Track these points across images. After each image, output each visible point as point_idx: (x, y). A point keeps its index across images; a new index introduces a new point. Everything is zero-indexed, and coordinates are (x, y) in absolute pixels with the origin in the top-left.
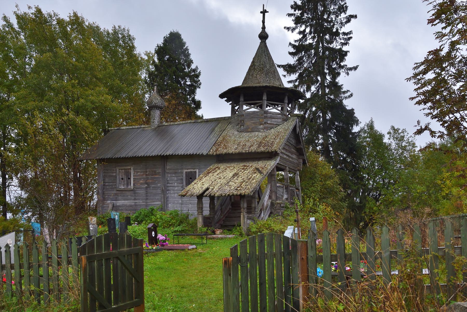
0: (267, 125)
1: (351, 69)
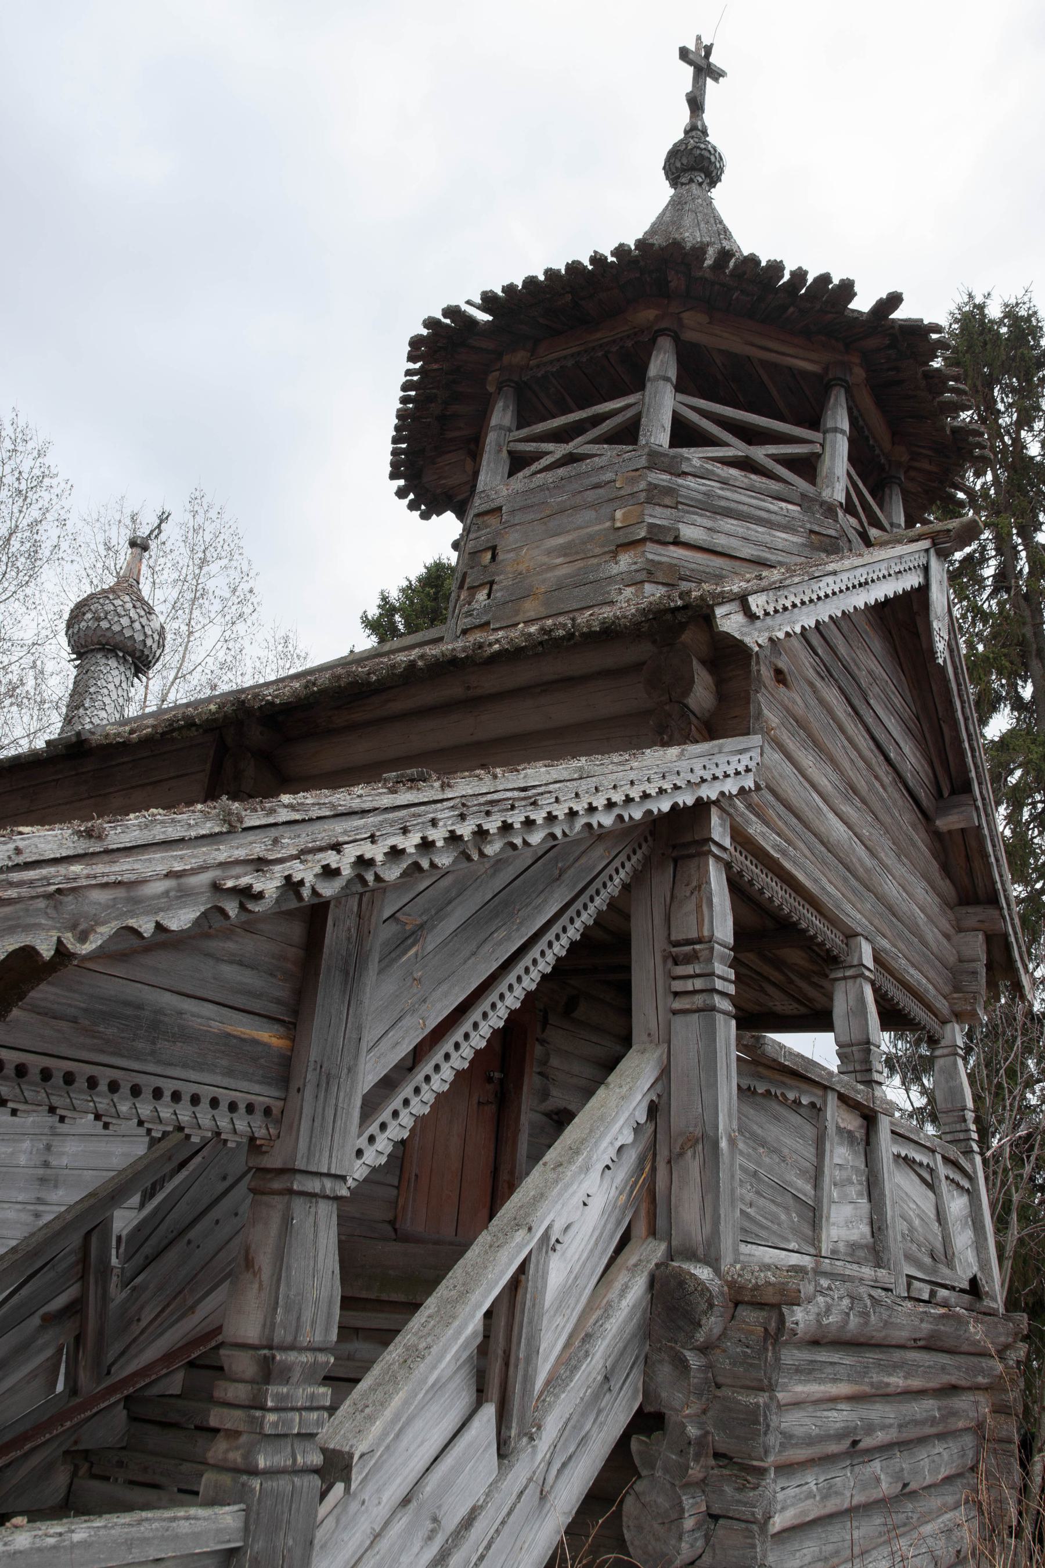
0: (677, 553)
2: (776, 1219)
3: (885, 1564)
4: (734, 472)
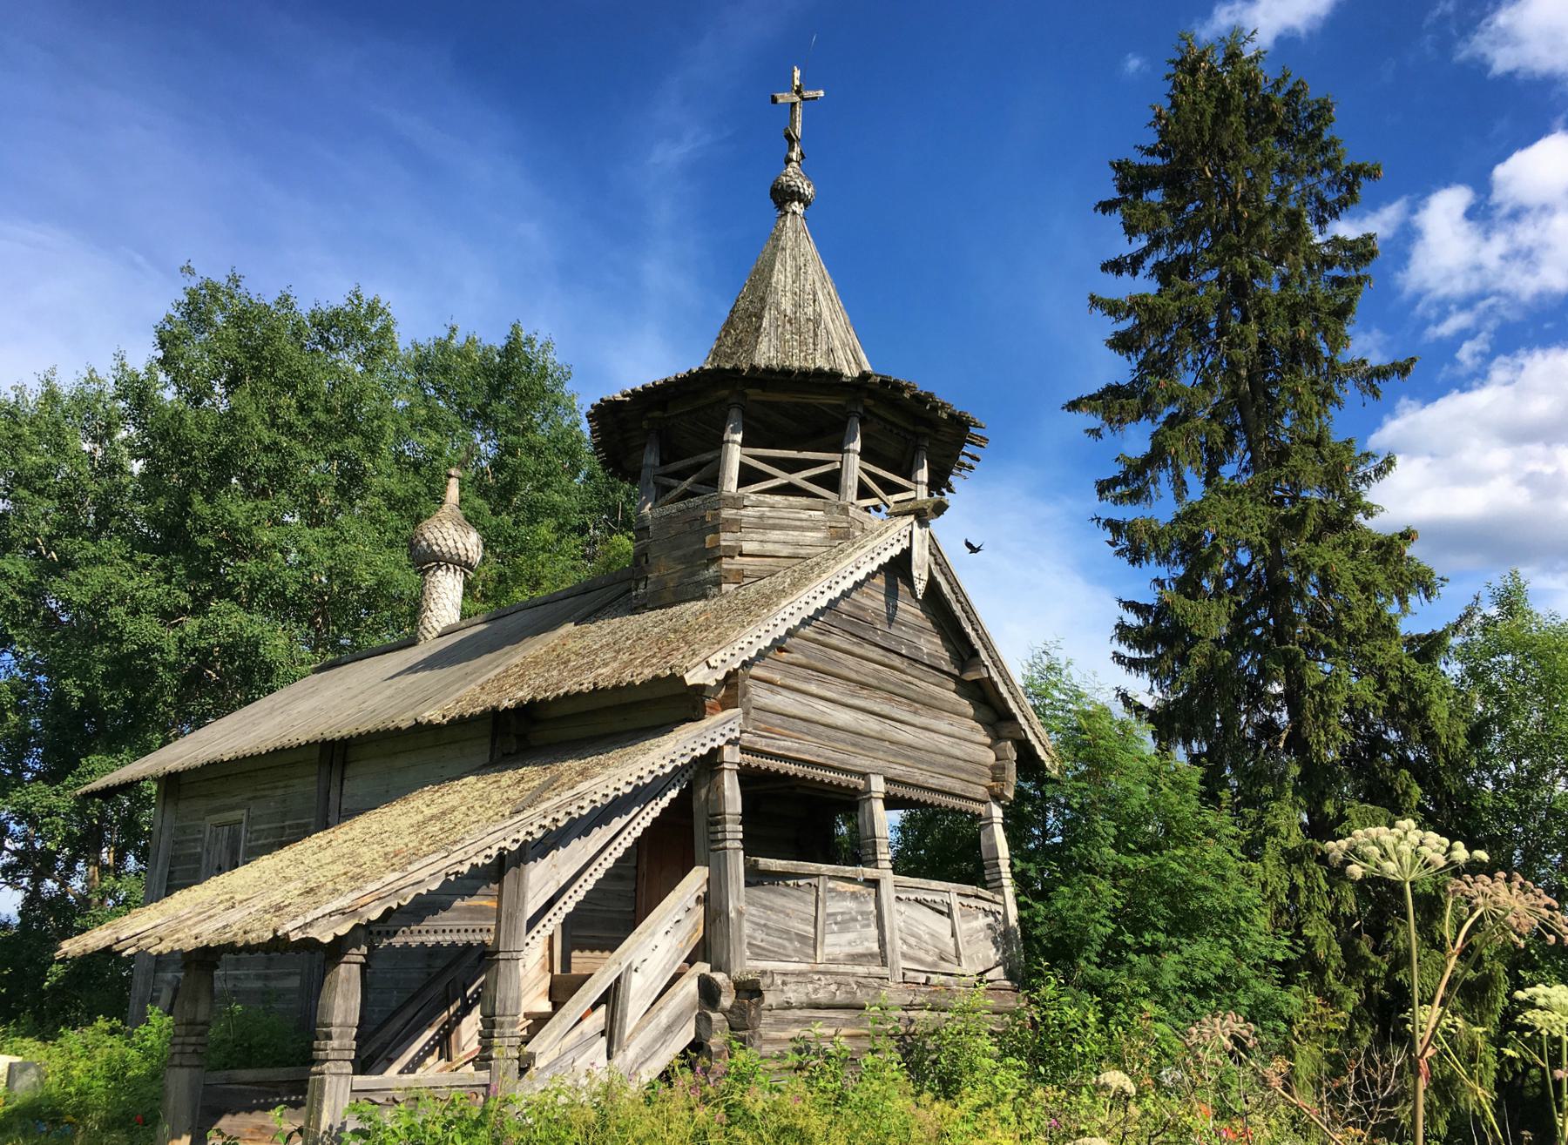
1: (1381, 373)
2: (784, 948)
3: (1559, 994)
4: (778, 498)
